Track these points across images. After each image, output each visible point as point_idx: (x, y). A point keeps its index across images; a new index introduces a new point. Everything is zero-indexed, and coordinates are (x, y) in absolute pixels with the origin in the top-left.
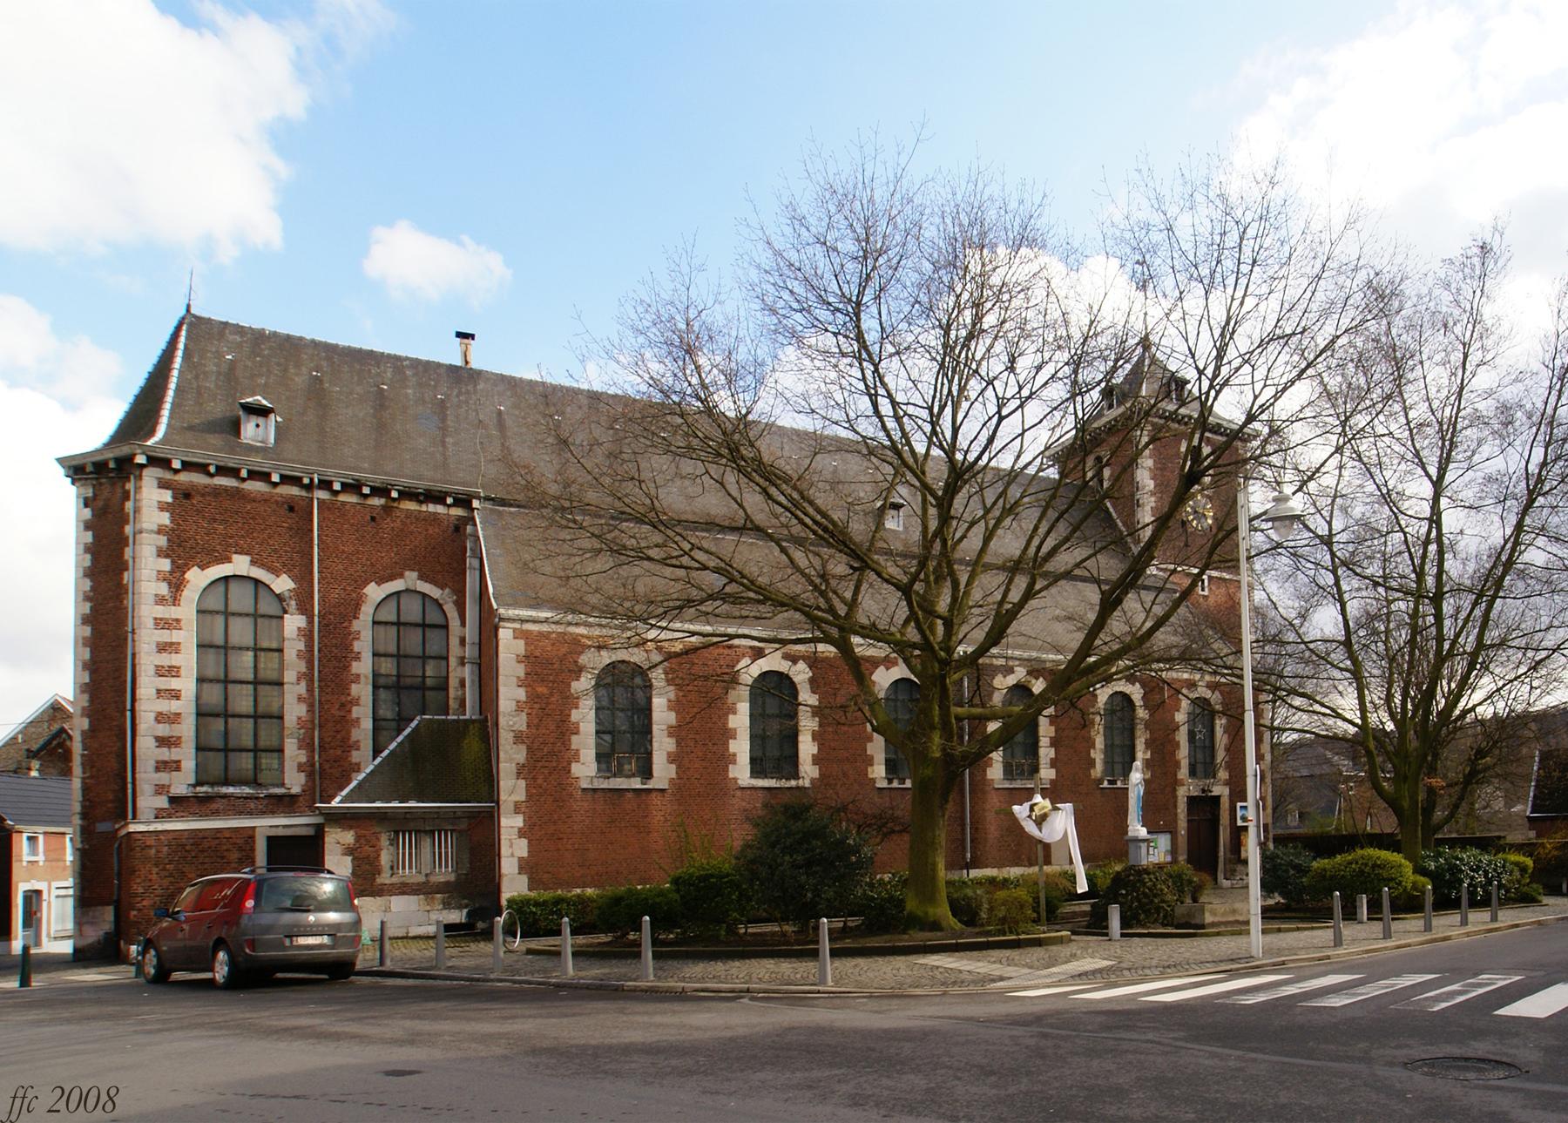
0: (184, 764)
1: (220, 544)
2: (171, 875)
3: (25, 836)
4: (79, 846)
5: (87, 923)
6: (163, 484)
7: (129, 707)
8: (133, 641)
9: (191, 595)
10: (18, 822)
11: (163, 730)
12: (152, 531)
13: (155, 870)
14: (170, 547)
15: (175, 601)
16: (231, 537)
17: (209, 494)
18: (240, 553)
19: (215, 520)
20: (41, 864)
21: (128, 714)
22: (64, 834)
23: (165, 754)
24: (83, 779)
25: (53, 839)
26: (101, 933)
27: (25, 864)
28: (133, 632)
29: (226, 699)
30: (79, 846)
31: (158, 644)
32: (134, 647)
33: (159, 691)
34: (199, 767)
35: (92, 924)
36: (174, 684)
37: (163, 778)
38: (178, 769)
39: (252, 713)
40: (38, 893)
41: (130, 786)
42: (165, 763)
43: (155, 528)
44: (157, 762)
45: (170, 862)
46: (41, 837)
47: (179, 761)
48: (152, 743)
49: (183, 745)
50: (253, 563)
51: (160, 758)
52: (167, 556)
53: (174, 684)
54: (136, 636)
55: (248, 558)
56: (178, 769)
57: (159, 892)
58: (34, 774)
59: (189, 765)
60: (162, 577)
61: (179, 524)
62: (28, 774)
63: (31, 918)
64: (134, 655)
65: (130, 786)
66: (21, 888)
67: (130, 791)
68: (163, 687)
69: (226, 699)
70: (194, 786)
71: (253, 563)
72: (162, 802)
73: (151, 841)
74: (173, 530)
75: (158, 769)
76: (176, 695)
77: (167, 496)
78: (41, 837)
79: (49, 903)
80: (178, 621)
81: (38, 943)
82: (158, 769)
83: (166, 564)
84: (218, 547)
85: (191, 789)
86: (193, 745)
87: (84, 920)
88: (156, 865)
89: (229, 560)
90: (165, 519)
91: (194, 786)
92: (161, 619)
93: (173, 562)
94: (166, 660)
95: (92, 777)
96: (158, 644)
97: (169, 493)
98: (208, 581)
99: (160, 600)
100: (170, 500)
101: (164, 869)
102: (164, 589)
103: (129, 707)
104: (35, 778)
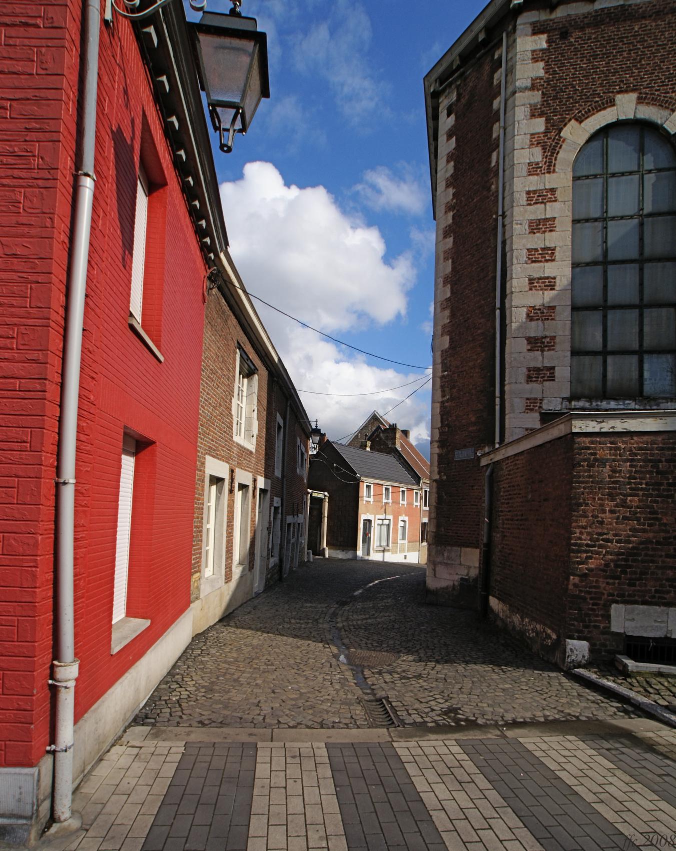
0: (558, 372)
1: (601, 85)
2: (634, 517)
3: (365, 484)
4: (437, 477)
5: (440, 563)
6: (537, 29)
7: (498, 305)
8: (504, 226)
9: (567, 156)
10: (362, 476)
11: (536, 329)
12: (526, 88)
13: (609, 504)
14: (545, 103)
15: (550, 168)
16: (614, 74)
17: (589, 25)
18: (626, 91)
19: (595, 56)
20: (372, 503)
21: (498, 312)
22: (382, 485)
23: (537, 359)
24: (442, 403)
25: (378, 488)
26: (457, 578)
27: (364, 502)
28: (504, 216)
29: (605, 287)
30: (437, 477)
31: (531, 222)
32: (504, 233)
33: (531, 281)
34: (576, 379)
35: (447, 564)
36: (549, 269)
37: (534, 390)
38: (552, 378)
39: (637, 301)
40: (370, 521)
41: (498, 401)
42: (537, 370)
43: (528, 83)
44: (529, 370)
45: (634, 492)
46: (372, 486)
47: (553, 368)
48: (524, 345)
49: (557, 347)
50: (640, 100)
51: (532, 365)
52: (541, 115)
53: (549, 269)
54: (507, 221)
55: (634, 96)
56: (552, 378)
57: (614, 546)
58: (368, 449)
59: (563, 372)
60: (536, 140)
61: (555, 72)
62: (365, 449)
63: (367, 539)
64: (504, 243)
65: (498, 401)
66: (362, 517)
67: (497, 408)
68: (536, 275)
69: (605, 287)
70: (570, 400)
71: (640, 100)
72: (534, 420)
73: (604, 452)
74: (548, 81)
75: (529, 379)
76: (549, 283)
77: (542, 41)
78: (372, 486)
79: (374, 528)
80: (553, 191)
81: (368, 554)
82: (529, 379)
83: (540, 125)
84: (599, 90)
85: (566, 403)
86: (568, 347)
87: (439, 559)
88: (612, 497)
89: (612, 103)
90: (539, 70)
91: (570, 400)
92: (535, 192)
93: (548, 121)
94: (538, 241)
95: (451, 399)
96: (531, 222)
97: (544, 37)
98: (586, 137)
99: (534, 169)
100: (545, 45)
101: (623, 504)
102: (537, 155)
103: (498, 305)
104: (368, 451)
